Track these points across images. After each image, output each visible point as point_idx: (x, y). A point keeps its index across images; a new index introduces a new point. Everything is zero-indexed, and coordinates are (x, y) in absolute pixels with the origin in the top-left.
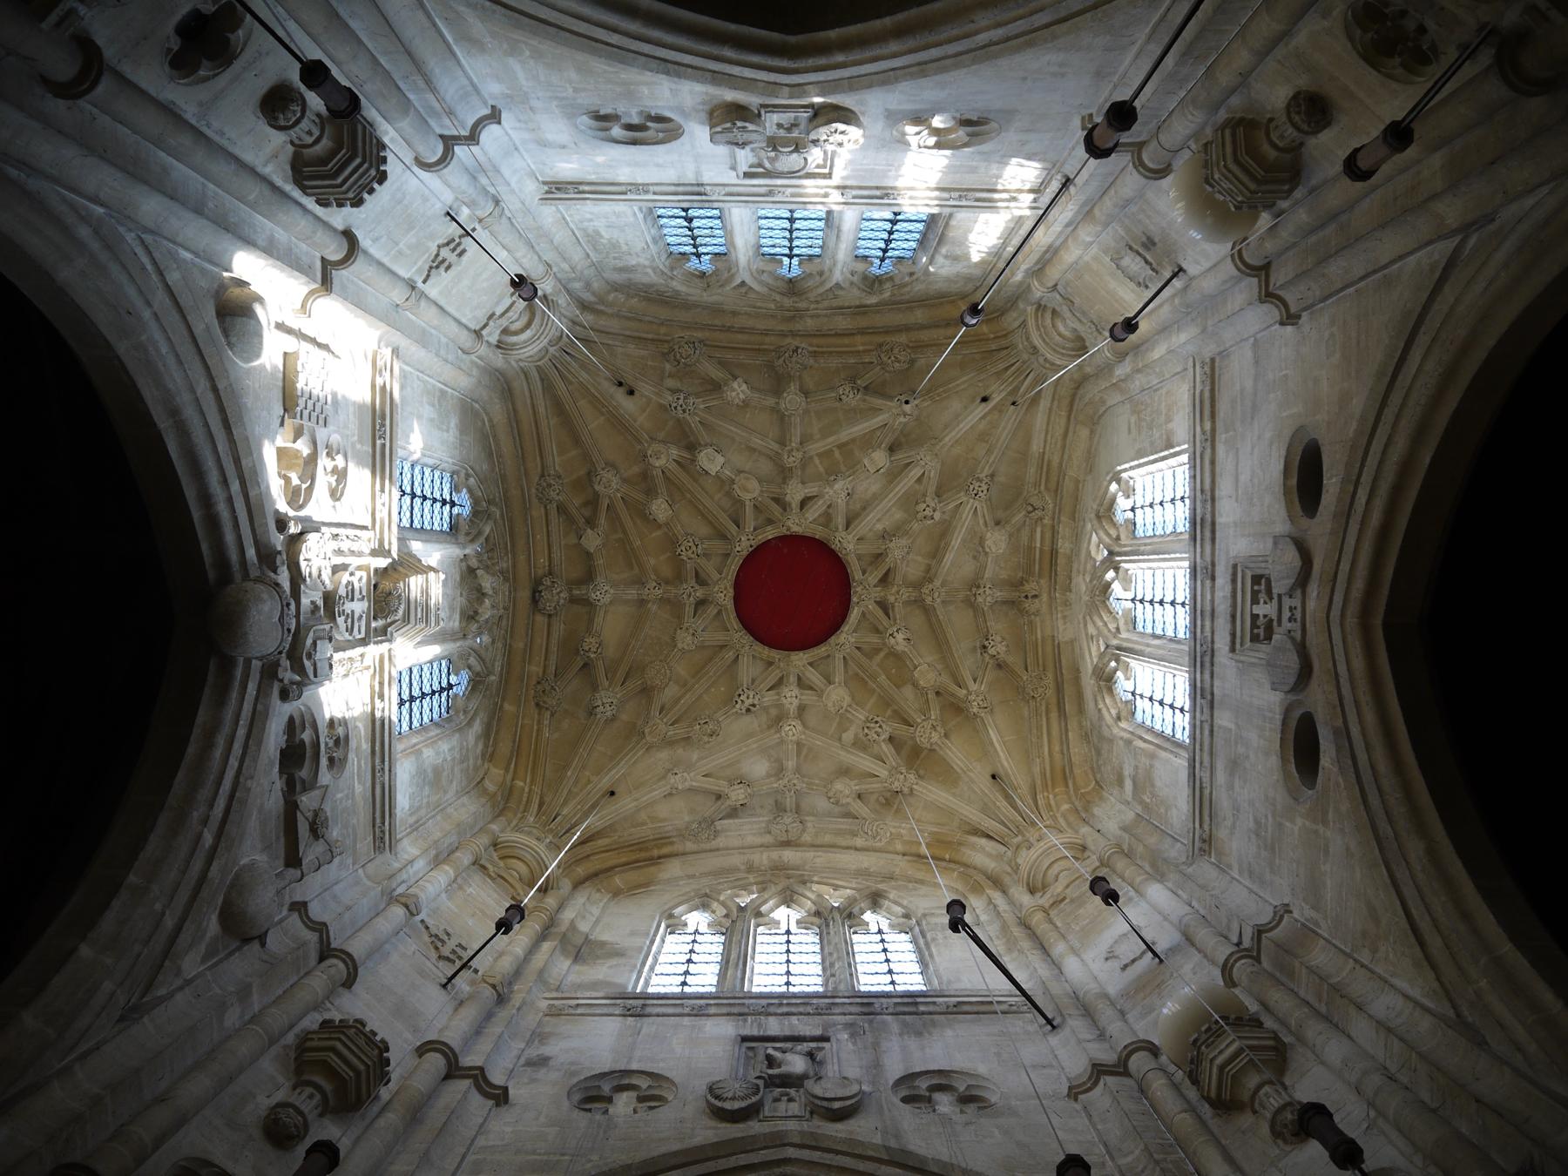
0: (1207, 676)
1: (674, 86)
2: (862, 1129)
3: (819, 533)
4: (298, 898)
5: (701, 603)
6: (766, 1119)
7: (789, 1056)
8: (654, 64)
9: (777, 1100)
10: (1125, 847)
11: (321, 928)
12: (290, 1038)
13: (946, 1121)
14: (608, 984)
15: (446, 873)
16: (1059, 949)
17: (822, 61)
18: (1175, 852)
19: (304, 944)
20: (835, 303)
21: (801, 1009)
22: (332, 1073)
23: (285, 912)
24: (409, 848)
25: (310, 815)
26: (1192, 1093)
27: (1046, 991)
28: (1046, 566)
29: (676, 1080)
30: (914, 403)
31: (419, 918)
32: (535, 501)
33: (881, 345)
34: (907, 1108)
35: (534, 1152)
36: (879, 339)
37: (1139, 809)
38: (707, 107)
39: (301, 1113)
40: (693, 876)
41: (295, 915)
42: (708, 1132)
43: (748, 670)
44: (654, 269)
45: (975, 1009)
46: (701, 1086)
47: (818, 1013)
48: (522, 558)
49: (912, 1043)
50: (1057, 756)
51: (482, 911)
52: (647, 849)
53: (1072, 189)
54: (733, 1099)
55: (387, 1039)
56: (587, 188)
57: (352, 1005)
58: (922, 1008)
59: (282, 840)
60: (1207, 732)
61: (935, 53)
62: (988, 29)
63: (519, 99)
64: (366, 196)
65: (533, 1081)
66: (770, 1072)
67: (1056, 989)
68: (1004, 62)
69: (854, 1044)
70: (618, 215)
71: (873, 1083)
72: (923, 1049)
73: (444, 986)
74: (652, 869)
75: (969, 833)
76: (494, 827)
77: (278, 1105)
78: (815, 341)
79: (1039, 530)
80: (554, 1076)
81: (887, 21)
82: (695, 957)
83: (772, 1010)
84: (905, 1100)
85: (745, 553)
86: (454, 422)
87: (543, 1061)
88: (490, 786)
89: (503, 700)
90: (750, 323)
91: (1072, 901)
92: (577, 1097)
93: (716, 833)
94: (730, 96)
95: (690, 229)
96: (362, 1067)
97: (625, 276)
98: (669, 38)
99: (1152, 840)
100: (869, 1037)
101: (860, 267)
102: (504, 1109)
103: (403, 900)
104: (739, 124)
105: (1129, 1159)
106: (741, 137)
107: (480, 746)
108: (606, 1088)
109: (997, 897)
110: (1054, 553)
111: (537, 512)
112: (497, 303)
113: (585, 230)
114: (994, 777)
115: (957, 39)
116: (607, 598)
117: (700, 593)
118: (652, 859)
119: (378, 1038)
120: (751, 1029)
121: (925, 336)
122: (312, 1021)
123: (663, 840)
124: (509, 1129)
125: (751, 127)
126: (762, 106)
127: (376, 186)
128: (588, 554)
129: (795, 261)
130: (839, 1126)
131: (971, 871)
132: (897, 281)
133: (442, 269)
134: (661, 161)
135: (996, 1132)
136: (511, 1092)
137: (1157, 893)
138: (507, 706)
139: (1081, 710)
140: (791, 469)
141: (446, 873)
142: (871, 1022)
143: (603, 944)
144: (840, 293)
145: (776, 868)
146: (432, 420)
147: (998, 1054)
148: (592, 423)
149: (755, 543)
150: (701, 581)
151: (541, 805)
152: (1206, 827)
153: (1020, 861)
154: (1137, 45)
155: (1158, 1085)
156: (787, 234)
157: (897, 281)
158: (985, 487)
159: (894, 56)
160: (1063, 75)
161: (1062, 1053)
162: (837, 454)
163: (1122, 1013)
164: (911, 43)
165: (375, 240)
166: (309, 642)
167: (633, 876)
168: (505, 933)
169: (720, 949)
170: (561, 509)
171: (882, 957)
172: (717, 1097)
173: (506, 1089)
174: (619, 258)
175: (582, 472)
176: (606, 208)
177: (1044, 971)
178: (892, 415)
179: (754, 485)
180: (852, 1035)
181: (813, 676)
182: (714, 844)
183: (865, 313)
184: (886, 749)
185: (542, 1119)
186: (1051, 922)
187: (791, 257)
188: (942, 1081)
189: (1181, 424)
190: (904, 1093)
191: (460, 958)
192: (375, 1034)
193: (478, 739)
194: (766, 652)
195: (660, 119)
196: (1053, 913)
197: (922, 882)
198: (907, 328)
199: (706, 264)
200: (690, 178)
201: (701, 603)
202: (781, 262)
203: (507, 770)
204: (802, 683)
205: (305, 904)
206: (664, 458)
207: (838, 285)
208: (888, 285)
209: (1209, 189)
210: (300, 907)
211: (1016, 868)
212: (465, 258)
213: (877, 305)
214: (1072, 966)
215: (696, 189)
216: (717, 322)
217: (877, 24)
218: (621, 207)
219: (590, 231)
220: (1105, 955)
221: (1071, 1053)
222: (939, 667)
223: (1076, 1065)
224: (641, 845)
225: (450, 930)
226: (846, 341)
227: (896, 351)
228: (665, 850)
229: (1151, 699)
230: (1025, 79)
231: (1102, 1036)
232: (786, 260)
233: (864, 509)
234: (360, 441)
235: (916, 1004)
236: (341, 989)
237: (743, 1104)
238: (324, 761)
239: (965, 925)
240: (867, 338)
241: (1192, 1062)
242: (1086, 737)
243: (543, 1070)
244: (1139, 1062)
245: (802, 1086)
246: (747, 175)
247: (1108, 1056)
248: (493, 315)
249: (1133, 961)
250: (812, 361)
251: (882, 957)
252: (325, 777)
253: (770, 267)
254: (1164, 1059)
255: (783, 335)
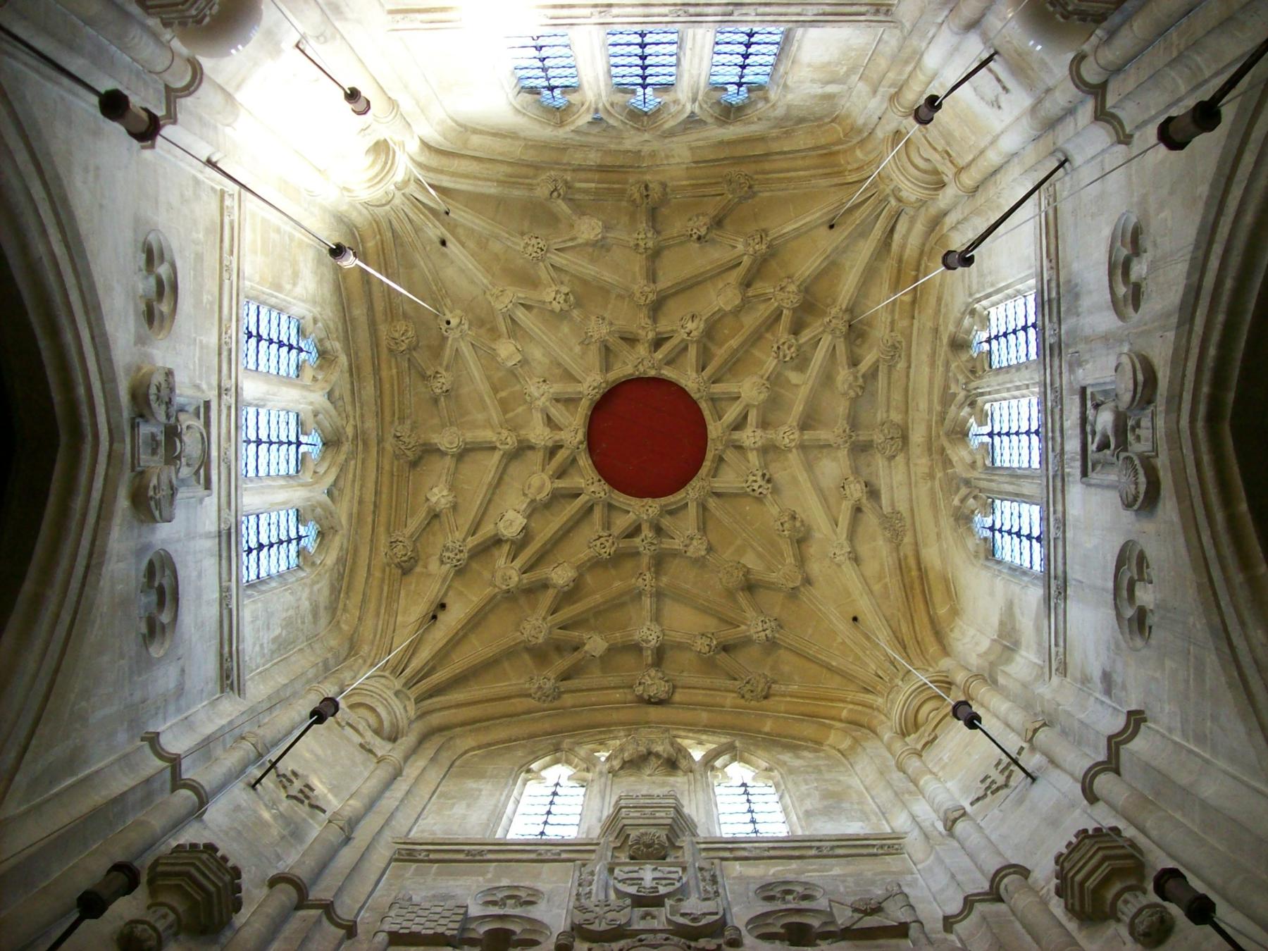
0: (710, 10)
1: (114, 559)
2: (1161, 353)
3: (584, 409)
4: (940, 925)
5: (658, 530)
6: (1155, 448)
7: (1099, 428)
8: (91, 578)
9: (1138, 438)
10: (893, 91)
11: (969, 903)
12: (1072, 926)
13: (1153, 267)
14: (1037, 615)
15: (926, 783)
16: (993, 157)
17: (85, 410)
18: (892, 39)
19: (984, 918)
20: (347, 398)
21: (1057, 417)
22: (1106, 882)
23: (952, 937)
24: (900, 821)
25: (857, 915)
26: (1116, 18)
27: (1033, 168)
28: (614, 176)
29: (1122, 542)
30: (449, 316)
31: (968, 808)
32: (557, 703)
33: (390, 350)
34: (1145, 307)
35: (1187, 681)
36: (384, 354)
37: (855, 78)
38: (136, 523)
39: (1140, 911)
40: (938, 535)
41: (957, 927)
42: (1168, 507)
43: (728, 480)
44: (314, 583)
45: (1053, 240)
46: (1128, 516)
47: (1059, 400)
48: (615, 716)
49: (1085, 303)
50: (808, 162)
51: (966, 746)
52: (912, 583)
53: (214, 159)
54: (1136, 484)
55: (1075, 831)
56: (226, 649)
57: (1044, 871)
58: (1054, 295)
59: (881, 942)
60: (767, 10)
61: (74, 297)
62: (48, 243)
63: (134, 716)
64: (230, 864)
65: (1124, 687)
66: (1112, 446)
67: (1030, 156)
68: (84, 227)
69: (1087, 361)
70: (255, 618)
71: (1121, 342)
72: (1090, 292)
73: (1034, 779)
74: (932, 576)
75: (889, 251)
76: (887, 736)
77: (1132, 934)
78: (388, 418)
79: (578, 185)
80: (1119, 666)
81: (43, 344)
82: (1015, 529)
83: (1058, 449)
84: (1136, 307)
85: (606, 487)
86: (471, 784)
87: (1107, 678)
88: (846, 744)
89: (760, 732)
90: (371, 485)
91: (948, 144)
92: (1139, 642)
93: (896, 512)
94: (123, 503)
95: (271, 545)
96: (1100, 854)
97: (322, 612)
98: (64, 563)
99: (883, 63)
100: (1081, 347)
101: (308, 373)
102: (1148, 714)
103: (949, 823)
104: (151, 493)
105: (1180, 81)
106: (165, 491)
107: (806, 754)
108: (1129, 612)
109: (950, 220)
110: (601, 169)
111: (568, 700)
112: (349, 740)
113: (273, 652)
114: (832, 227)
115: (59, 274)
116: (656, 628)
117: (647, 532)
118: (921, 578)
119: (1074, 840)
120: (1074, 469)
121: (379, 306)
122: (1057, 907)
123: (901, 566)
124: (1167, 708)
125: (154, 482)
126: (133, 469)
127: (219, 854)
128: (609, 650)
129: (303, 439)
130: (1160, 375)
131: (927, 249)
132: (323, 335)
133: (310, 794)
134: (194, 574)
135: (1162, 215)
136: (1133, 707)
137: (932, 59)
138: (767, 729)
139: (762, 139)
140: (519, 442)
141: (926, 783)
142: (1068, 346)
143: (1002, 623)
144: (337, 394)
145: (930, 449)
146: (469, 806)
147: (1093, 216)
148: (476, 650)
149: (596, 477)
150: (635, 531)
151: (867, 691)
152: (863, 9)
153: (913, 198)
154: (65, 95)
155: (1111, 55)
156: (274, 447)
157: (323, 335)
158: (534, 241)
159: (77, 337)
160: (97, 168)
161: (1091, 151)
162: (503, 394)
163: (1048, 91)
164: (64, 321)
165: (279, 858)
166: (682, 920)
167: (938, 596)
168: (979, 720)
169: (1007, 503)
170: (565, 676)
171: (1011, 337)
172: (1135, 499)
173: (1130, 713)
174: (303, 618)
175: (526, 657)
176: (248, 631)
177: (1015, 170)
178: (461, 340)
179: (536, 481)
180: (1080, 364)
181: (732, 413)
182: (906, 514)
183: (358, 368)
184: (805, 336)
185: (1158, 675)
186: (969, 165)
187: (299, 444)
188: (1119, 268)
189: (42, 81)
190: (1130, 310)
191: (1009, 764)
192: (1070, 843)
193: (798, 757)
194: (707, 464)
195: (151, 571)
196: (961, 163)
197: (939, 300)
198: (373, 324)
199: (309, 530)
200: (212, 544)
201: (658, 530)
202: (304, 454)
203: (831, 727)
204: (739, 425)
205: (946, 918)
206: (506, 571)
207: (330, 395)
208: (328, 345)
209: (207, 20)
210: (949, 923)
211: (922, 203)
212: (300, 771)
213: (349, 355)
214: (1009, 143)
215: (224, 538)
216: (370, 520)
217: (47, 355)
218: (247, 614)
219: (274, 647)
220: (995, 110)
221: (1089, 142)
222: (721, 285)
223: (1100, 136)
224: (907, 589)
225: (982, 777)
226: (387, 386)
227: (396, 335)
228: (912, 562)
229: (743, 67)
230: (101, 206)
231: (1070, 111)
232: (303, 449)
233: (559, 365)
234: (483, 874)
235: (1049, 300)
236: (1030, 880)
237: (1141, 472)
238: (805, 905)
239: (967, 250)
240: (384, 366)
241: (1084, 20)
242: (788, 134)
243: (1115, 676)
244: (1091, 73)
245: (1125, 414)
246: (208, 486)
247: (1089, 106)
248: (361, 746)
249: (999, 80)
250: (408, 422)
251: (1011, 337)
252: (822, 903)
253: (310, 466)
254: (1086, 47)
255: (381, 451)
